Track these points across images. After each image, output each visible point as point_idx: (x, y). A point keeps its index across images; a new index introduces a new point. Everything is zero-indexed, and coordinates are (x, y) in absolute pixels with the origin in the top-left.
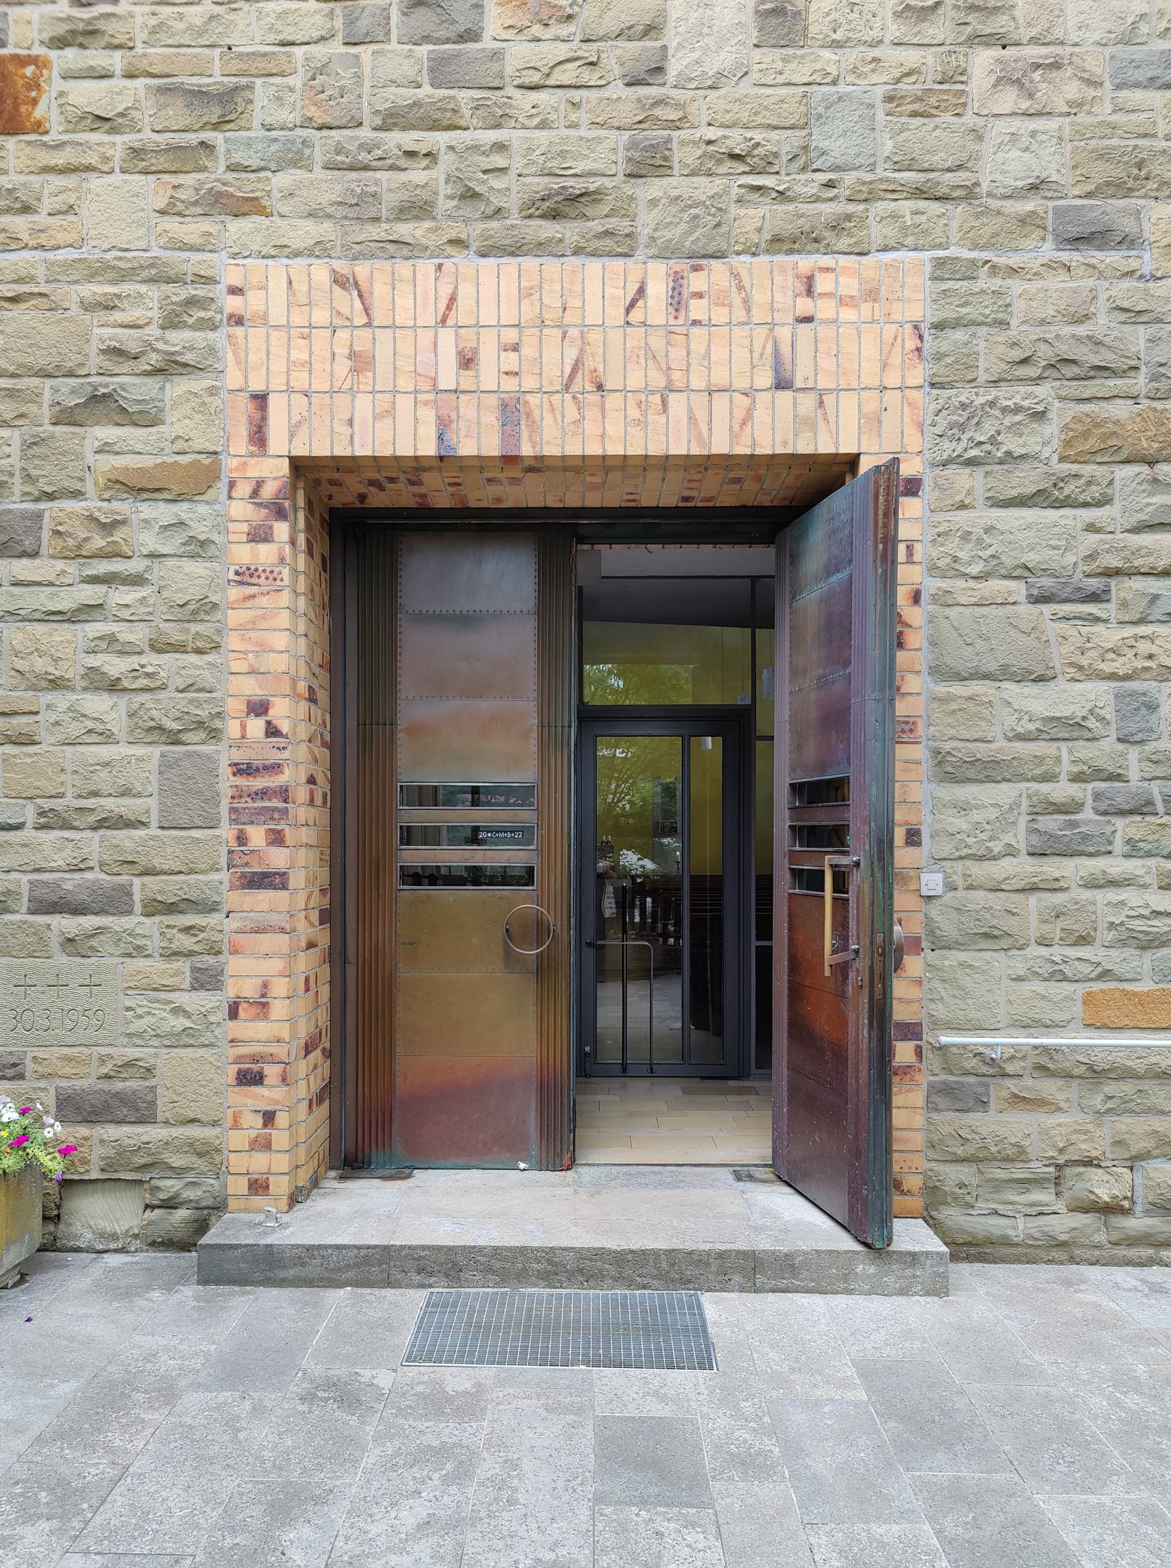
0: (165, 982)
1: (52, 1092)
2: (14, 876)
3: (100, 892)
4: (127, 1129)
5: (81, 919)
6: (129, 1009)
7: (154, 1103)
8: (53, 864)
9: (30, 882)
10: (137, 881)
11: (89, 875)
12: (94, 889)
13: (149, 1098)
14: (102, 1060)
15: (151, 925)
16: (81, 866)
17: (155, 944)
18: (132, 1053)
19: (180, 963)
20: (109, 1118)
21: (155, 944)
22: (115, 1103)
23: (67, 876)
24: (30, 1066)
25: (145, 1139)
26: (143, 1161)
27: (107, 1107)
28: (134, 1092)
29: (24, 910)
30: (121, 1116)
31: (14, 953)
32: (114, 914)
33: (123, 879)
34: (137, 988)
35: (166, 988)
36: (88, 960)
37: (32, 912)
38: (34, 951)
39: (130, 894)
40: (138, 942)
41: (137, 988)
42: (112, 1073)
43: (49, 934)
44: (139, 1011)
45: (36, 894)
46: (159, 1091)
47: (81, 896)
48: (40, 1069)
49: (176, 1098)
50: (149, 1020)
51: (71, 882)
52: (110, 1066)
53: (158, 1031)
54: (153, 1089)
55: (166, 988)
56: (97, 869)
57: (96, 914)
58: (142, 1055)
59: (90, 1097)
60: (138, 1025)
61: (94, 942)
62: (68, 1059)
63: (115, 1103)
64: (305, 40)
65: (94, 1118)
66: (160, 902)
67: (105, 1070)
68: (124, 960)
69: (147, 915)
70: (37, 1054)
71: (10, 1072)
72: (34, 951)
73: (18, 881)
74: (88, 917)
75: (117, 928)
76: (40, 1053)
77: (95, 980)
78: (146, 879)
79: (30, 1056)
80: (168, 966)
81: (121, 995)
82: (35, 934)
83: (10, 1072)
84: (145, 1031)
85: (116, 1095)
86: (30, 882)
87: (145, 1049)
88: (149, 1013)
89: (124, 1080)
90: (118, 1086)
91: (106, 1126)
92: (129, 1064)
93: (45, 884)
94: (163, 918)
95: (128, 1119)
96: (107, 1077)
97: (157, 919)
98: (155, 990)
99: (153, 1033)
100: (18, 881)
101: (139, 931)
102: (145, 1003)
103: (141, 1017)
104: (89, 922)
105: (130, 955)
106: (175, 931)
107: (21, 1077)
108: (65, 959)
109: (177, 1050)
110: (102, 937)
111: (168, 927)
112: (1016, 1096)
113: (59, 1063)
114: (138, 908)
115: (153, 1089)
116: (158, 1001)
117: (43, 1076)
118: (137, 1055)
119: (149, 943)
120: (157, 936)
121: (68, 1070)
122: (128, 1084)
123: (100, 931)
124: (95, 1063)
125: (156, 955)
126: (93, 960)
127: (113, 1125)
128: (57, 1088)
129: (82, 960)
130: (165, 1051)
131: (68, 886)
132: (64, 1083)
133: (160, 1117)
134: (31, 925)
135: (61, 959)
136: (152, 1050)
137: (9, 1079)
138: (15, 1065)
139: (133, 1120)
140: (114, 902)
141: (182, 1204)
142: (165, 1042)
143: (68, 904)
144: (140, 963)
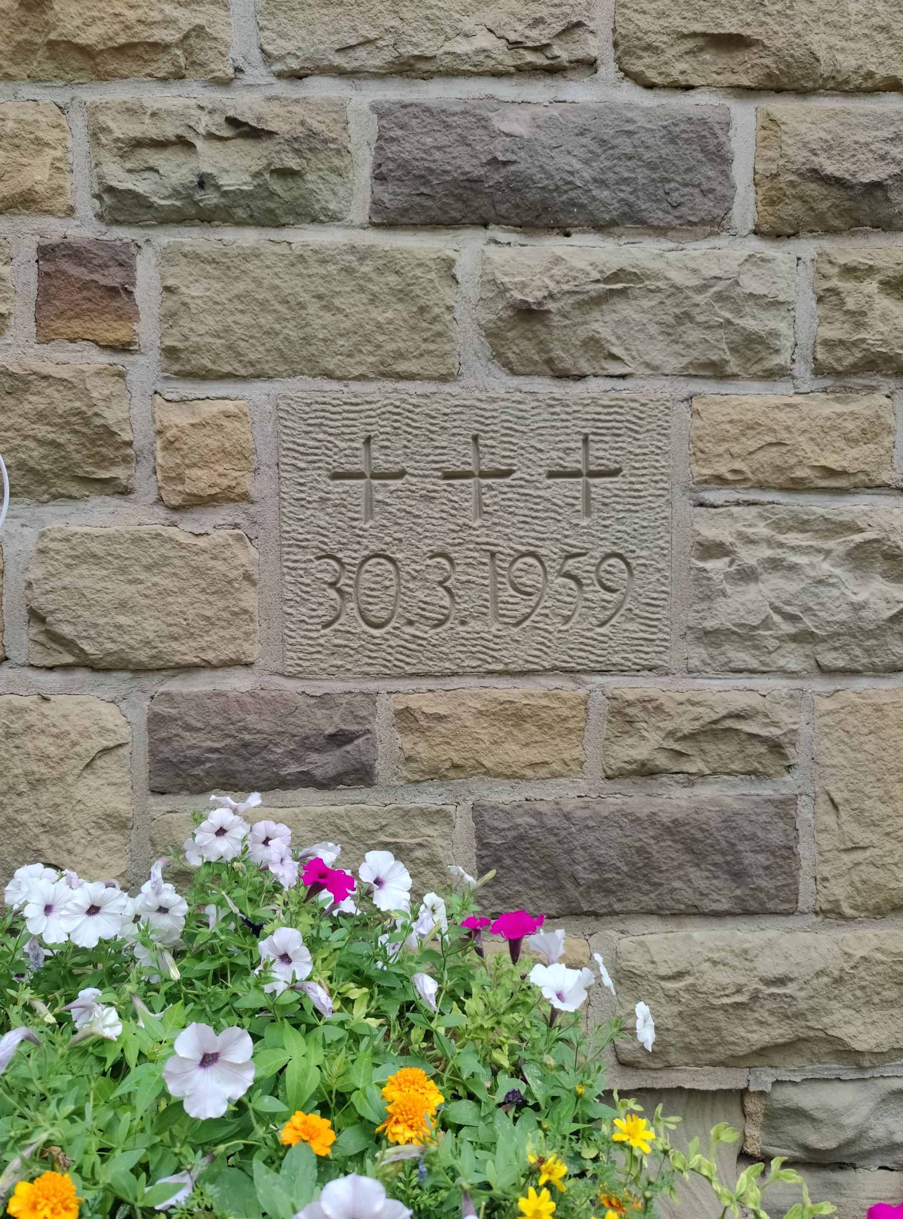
0: (832, 461)
1: (464, 823)
2: (320, 89)
3: (625, 145)
4: (703, 937)
5: (554, 245)
6: (712, 549)
7: (789, 852)
8: (462, 47)
9: (381, 112)
10: (744, 116)
11: (579, 92)
12: (603, 137)
13: (776, 837)
14: (623, 717)
15: (791, 268)
16: (562, 52)
17: (801, 329)
18: (723, 694)
19: (879, 399)
20: (649, 901)
21: (801, 329)
22: (666, 853)
23: (504, 90)
24: (387, 744)
25: (770, 966)
26: (760, 1037)
27: (643, 867)
28: (729, 820)
29: (359, 211)
30: (688, 895)
31: (330, 363)
32: (661, 231)
33: (701, 103)
34: (738, 480)
35: (836, 482)
36: (576, 389)
37: (387, 220)
38: (400, 355)
39: (721, 158)
40: (750, 324)
41: (738, 480)
42: (662, 761)
43: (448, 294)
44: (749, 556)
45: (407, 149)
46: (804, 813)
47: (562, 160)
48: (422, 750)
49: (861, 836)
50: (774, 586)
51: (522, 111)
52: (655, 738)
53: (809, 623)
54: (785, 808)
55: (836, 482)
56: (608, 69)
57: (600, 227)
58: (754, 700)
59: (590, 838)
60: (743, 603)
61: (601, 324)
62: (515, 716)
63: (666, 853)
64: (85, 343)
65: (600, 902)
66: (837, 182)
67: (641, 748)
68: (696, 386)
69: (776, 235)
70: (414, 702)
71: (325, 763)
72: (400, 355)
73: (341, 107)
74: (577, 239)
75: (679, 278)
76: (424, 699)
77: (603, 453)
78: (782, 107)
79: (386, 706)
80: (839, 408)
81: (684, 506)
82: (403, 295)
83: (325, 763)
84: (766, 624)
85: (673, 830)
86: (381, 112)
87: (760, 683)
88: (775, 565)
89: (691, 779)
90: (674, 800)
91: (636, 925)
92: (714, 731)
93: (437, 116)
94: (829, 245)
95: (708, 905)
96: (646, 772)
97: (807, 247)
98: (797, 486)
99: (788, 628)
100: (341, 107)
101: (750, 284)
102: (762, 530)
103: (747, 575)
104: (587, 254)
105: (716, 371)
106: (871, 286)
107: (361, 775)
108: (501, 383)
109: (862, 684)
110: (626, 309)
111: (850, 272)
112: (480, 712)
113: (484, 731)
114: (745, 207)
115: (785, 808)
116: (803, 526)
117: (436, 774)
118: (740, 702)
119: (782, 327)
120: (806, 306)
121: (514, 753)
122: (706, 792)
123: (620, 285)
124: (598, 727)
125: (802, 370)
126: (595, 386)
127: (654, 924)
128: (477, 811)
129: (558, 389)
130: (820, 685)
131: (515, 123)
132: (501, 795)
133: (806, 901)
134: (389, 264)
135: (488, 384)
136: (781, 685)
137: (323, 785)
138: (340, 739)
139: (725, 906)
140: (667, 190)
141: (867, 1155)
142: (830, 659)
143: (517, 186)
144: (750, 398)
